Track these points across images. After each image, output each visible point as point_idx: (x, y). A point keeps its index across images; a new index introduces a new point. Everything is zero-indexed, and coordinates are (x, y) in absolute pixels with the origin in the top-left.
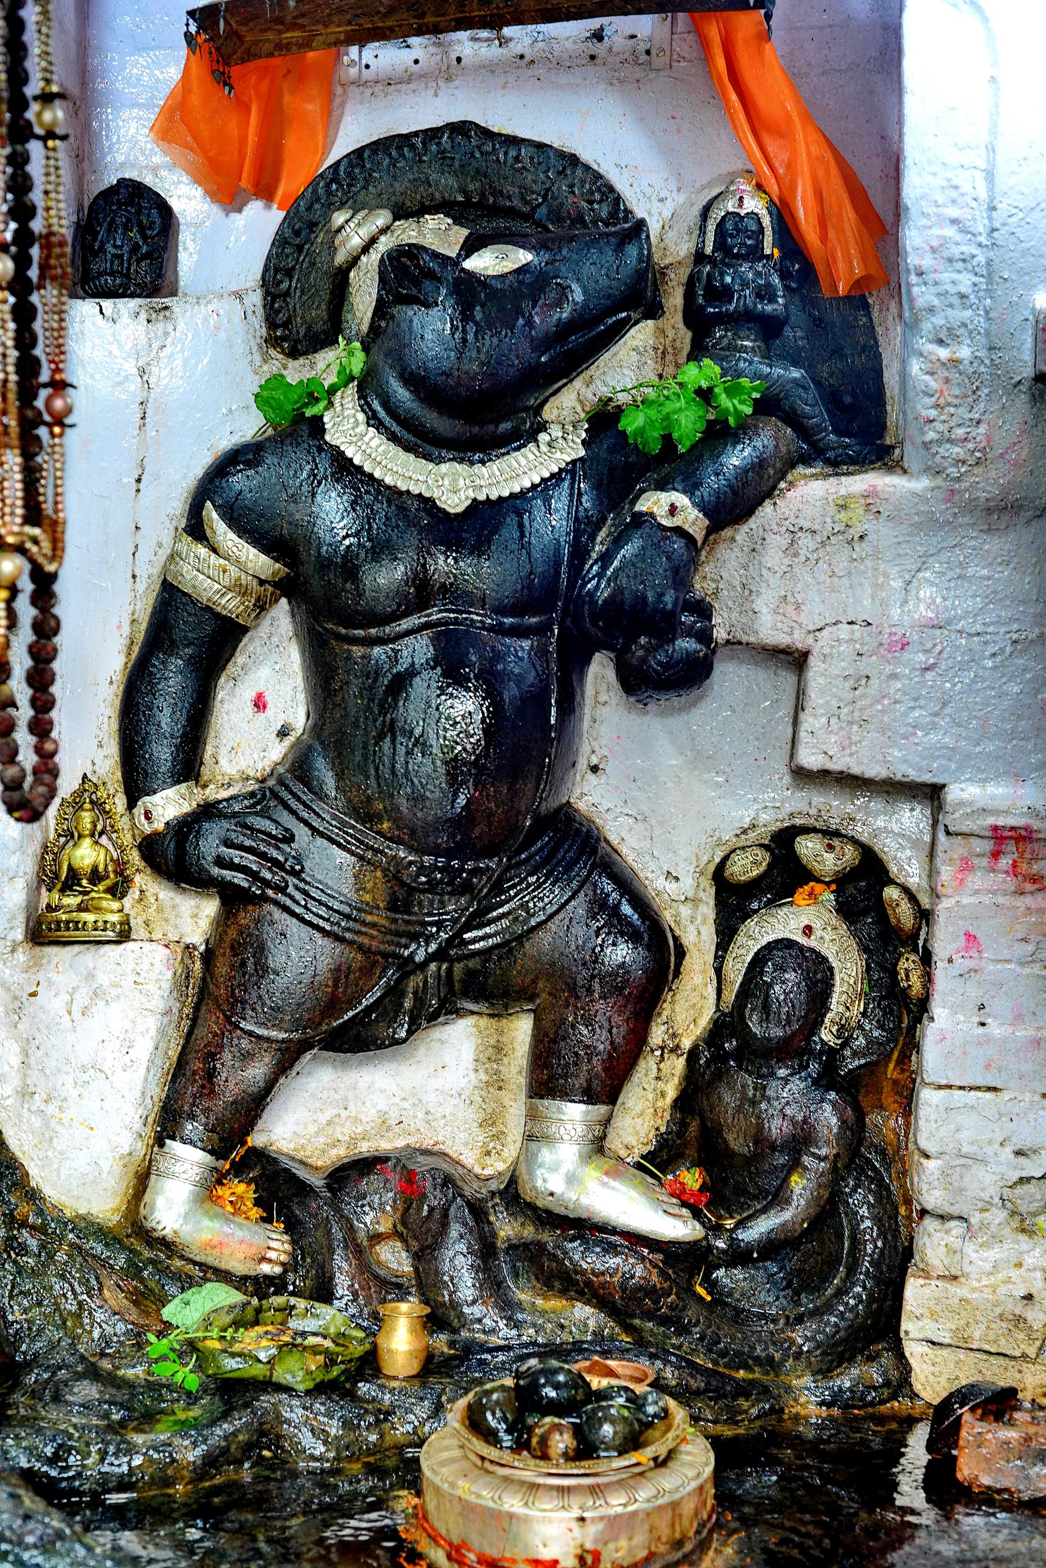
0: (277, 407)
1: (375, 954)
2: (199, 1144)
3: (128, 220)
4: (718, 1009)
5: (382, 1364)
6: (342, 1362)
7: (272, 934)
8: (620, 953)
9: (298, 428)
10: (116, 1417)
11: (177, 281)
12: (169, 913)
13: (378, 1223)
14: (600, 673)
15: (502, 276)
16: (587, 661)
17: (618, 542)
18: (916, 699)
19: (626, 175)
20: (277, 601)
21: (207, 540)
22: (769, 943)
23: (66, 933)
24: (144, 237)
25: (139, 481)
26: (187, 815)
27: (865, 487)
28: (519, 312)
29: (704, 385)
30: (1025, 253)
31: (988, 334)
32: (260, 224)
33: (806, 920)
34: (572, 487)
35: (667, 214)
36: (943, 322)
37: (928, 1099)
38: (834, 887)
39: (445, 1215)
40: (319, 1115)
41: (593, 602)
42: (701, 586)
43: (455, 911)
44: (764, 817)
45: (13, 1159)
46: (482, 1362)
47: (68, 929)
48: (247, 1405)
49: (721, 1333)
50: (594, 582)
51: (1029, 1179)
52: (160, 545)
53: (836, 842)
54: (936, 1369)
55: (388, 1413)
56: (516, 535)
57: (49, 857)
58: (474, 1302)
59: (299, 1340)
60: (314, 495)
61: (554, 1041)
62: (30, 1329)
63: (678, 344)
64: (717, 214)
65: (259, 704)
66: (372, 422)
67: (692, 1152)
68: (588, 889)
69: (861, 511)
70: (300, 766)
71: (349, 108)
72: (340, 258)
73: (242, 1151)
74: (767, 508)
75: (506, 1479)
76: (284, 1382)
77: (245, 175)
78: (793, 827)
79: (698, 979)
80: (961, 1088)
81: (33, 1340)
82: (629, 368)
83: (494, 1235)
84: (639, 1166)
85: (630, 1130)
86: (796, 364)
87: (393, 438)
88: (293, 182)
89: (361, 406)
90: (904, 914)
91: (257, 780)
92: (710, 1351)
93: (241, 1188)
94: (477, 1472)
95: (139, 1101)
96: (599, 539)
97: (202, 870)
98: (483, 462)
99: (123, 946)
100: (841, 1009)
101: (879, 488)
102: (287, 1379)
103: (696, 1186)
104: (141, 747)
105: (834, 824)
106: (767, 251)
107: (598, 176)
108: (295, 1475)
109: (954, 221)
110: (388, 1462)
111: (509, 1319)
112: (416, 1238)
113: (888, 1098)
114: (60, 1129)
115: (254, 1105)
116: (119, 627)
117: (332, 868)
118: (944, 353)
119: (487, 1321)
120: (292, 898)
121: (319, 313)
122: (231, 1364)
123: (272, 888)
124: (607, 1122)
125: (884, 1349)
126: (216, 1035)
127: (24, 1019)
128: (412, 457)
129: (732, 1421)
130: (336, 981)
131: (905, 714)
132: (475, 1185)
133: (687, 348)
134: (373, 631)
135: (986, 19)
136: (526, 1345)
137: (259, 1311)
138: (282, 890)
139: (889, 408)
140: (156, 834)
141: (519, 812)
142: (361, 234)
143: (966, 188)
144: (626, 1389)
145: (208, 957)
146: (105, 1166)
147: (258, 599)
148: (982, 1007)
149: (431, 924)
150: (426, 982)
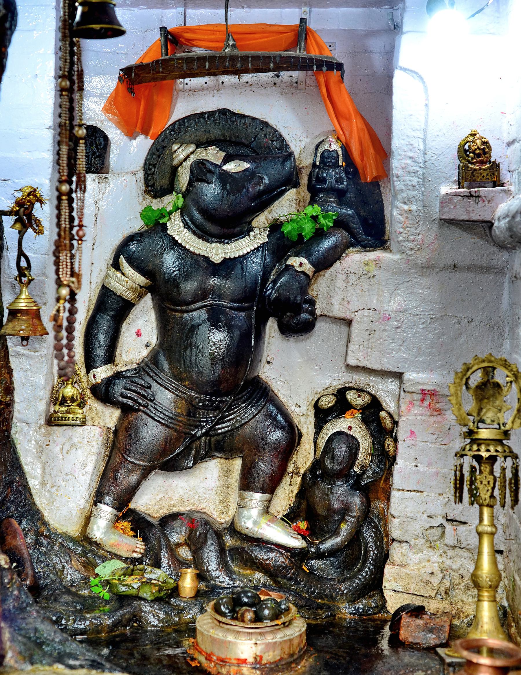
0: (149, 219)
1: (181, 433)
3: (92, 142)
4: (315, 458)
5: (180, 592)
7: (142, 424)
8: (277, 435)
9: (157, 227)
10: (78, 608)
11: (109, 165)
12: (101, 414)
14: (272, 326)
16: (267, 321)
17: (280, 275)
18: (393, 340)
19: (287, 130)
24: (97, 148)
25: (93, 245)
26: (109, 377)
27: (375, 257)
28: (244, 187)
29: (314, 214)
30: (437, 171)
31: (423, 201)
32: (142, 145)
33: (350, 424)
34: (262, 254)
35: (302, 146)
37: (395, 495)
38: (361, 411)
39: (206, 536)
40: (156, 496)
41: (269, 299)
42: (312, 293)
44: (334, 383)
45: (38, 509)
46: (220, 593)
48: (128, 605)
50: (270, 291)
51: (433, 527)
52: (101, 271)
53: (362, 394)
54: (396, 601)
55: (182, 610)
56: (240, 272)
57: (55, 392)
58: (216, 570)
60: (163, 254)
61: (250, 469)
63: (305, 198)
64: (321, 150)
65: (138, 334)
67: (303, 515)
68: (265, 409)
70: (154, 358)
71: (179, 100)
72: (175, 163)
73: (127, 509)
74: (337, 264)
75: (228, 629)
77: (138, 126)
78: (346, 387)
79: (307, 446)
80: (408, 491)
81: (46, 579)
83: (225, 545)
86: (351, 207)
87: (194, 233)
88: (157, 129)
90: (388, 422)
91: (137, 364)
92: (308, 592)
93: (126, 523)
94: (217, 627)
96: (272, 274)
98: (228, 243)
99: (83, 427)
100: (362, 459)
102: (144, 595)
103: (305, 528)
104: (93, 350)
105: (362, 386)
106: (340, 164)
108: (146, 631)
109: (411, 158)
110: (182, 629)
111: (230, 577)
112: (194, 545)
113: (380, 495)
114: (57, 498)
115: (132, 491)
116: (84, 302)
117: (165, 398)
118: (406, 207)
120: (150, 410)
121: (165, 182)
122: (123, 589)
124: (270, 501)
126: (118, 463)
128: (201, 241)
130: (166, 443)
131: (389, 345)
132: (217, 525)
133: (308, 201)
134: (184, 307)
135: (424, 83)
137: (133, 570)
138: (146, 407)
139: (386, 225)
140: (97, 384)
141: (239, 379)
142: (183, 153)
143: (416, 145)
145: (116, 432)
146: (74, 513)
147: (139, 294)
148: (416, 459)
150: (201, 444)
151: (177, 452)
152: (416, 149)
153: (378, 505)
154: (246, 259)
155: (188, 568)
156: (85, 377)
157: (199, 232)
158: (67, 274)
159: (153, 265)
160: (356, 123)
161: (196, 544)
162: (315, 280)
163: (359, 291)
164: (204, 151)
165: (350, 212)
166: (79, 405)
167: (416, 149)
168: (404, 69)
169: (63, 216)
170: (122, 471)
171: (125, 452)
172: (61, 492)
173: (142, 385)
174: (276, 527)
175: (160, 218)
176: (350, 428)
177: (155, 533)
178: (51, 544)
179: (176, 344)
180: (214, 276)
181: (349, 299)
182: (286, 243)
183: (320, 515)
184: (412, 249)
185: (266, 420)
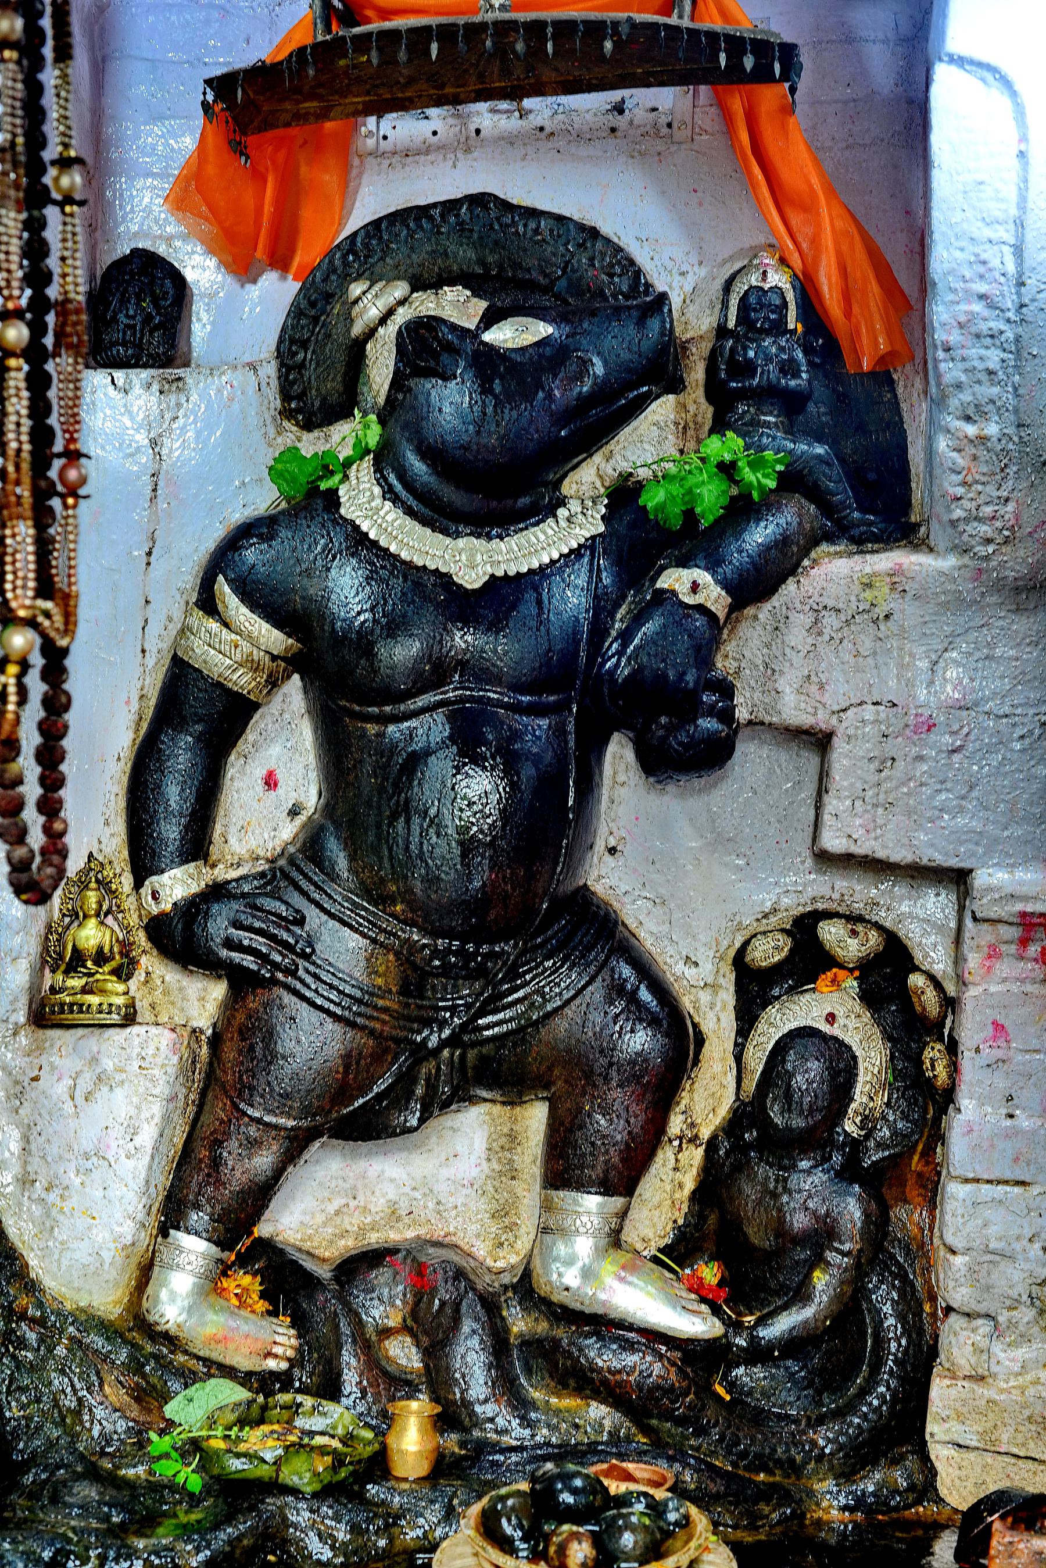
0: (292, 480)
1: (386, 1039)
2: (204, 1235)
3: (141, 290)
4: (738, 1099)
5: (392, 1465)
6: (350, 1463)
8: (639, 1040)
9: (314, 501)
11: (190, 351)
12: (175, 995)
13: (387, 1317)
14: (619, 756)
15: (522, 349)
16: (606, 742)
17: (638, 619)
19: (647, 248)
20: (289, 677)
21: (219, 614)
22: (791, 1031)
23: (70, 1016)
25: (149, 554)
26: (195, 896)
27: (890, 565)
28: (540, 386)
29: (728, 457)
31: (1016, 411)
32: (274, 295)
33: (831, 1007)
34: (591, 564)
35: (688, 288)
36: (970, 398)
40: (324, 1206)
42: (723, 665)
43: (469, 995)
44: (786, 901)
45: (13, 1249)
47: (72, 1012)
48: (252, 1508)
49: (741, 1435)
50: (614, 660)
52: (170, 619)
53: (860, 928)
56: (534, 611)
58: (486, 1401)
59: (306, 1440)
60: (328, 570)
61: (571, 1131)
62: (28, 1426)
64: (740, 288)
65: (270, 782)
66: (388, 496)
67: (710, 1246)
68: (605, 974)
69: (886, 590)
70: (311, 847)
72: (357, 330)
74: (790, 587)
76: (290, 1483)
79: (717, 1068)
80: (989, 1182)
81: (31, 1438)
82: (650, 443)
83: (507, 1330)
84: (655, 1260)
85: (647, 1222)
86: (820, 440)
87: (410, 512)
88: (309, 253)
89: (377, 480)
90: (930, 1000)
91: (267, 860)
93: (247, 1280)
95: (144, 1189)
96: (619, 616)
97: (211, 951)
99: (128, 1030)
100: (865, 1099)
101: (905, 567)
102: (294, 1480)
103: (714, 1281)
104: (149, 825)
105: (858, 907)
106: (791, 326)
107: (619, 249)
109: (982, 297)
111: (523, 1418)
112: (426, 1333)
113: (912, 1191)
114: (61, 1218)
115: (261, 1194)
116: (128, 703)
117: (343, 949)
118: (971, 430)
119: (500, 1421)
120: (302, 982)
121: (333, 385)
122: (236, 1464)
123: (282, 971)
124: (623, 1214)
125: (908, 1452)
126: (222, 1122)
127: (26, 1104)
128: (428, 531)
129: (753, 1528)
130: (347, 1067)
131: (932, 797)
133: (707, 428)
134: (388, 709)
135: (1014, 94)
136: (539, 1446)
137: (264, 1408)
138: (293, 973)
139: (913, 485)
140: (163, 915)
141: (536, 895)
142: (379, 306)
143: (995, 263)
144: (646, 1495)
145: (216, 1041)
146: (107, 1256)
147: (270, 676)
149: (445, 1009)
150: (439, 1069)
151: (376, 1089)
152: (997, 275)
153: (907, 1217)
154: (549, 576)
155: (410, 1397)
156: (132, 899)
157: (423, 510)
158: (24, 587)
159: (303, 598)
160: (829, 222)
161: (434, 1334)
162: (731, 631)
163: (847, 657)
164: (433, 297)
165: (820, 450)
166: (117, 972)
167: (997, 275)
168: (960, 61)
169: (13, 418)
170: (233, 1144)
171: (240, 1096)
172: (74, 1201)
173: (279, 916)
174: (641, 1284)
175: (321, 478)
176: (831, 1018)
177: (327, 1300)
178: (47, 1342)
179: (369, 804)
180: (466, 624)
181: (823, 678)
182: (653, 535)
183: (754, 1248)
184: (989, 541)
185: (611, 1003)
